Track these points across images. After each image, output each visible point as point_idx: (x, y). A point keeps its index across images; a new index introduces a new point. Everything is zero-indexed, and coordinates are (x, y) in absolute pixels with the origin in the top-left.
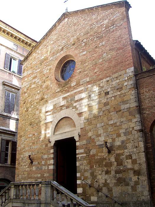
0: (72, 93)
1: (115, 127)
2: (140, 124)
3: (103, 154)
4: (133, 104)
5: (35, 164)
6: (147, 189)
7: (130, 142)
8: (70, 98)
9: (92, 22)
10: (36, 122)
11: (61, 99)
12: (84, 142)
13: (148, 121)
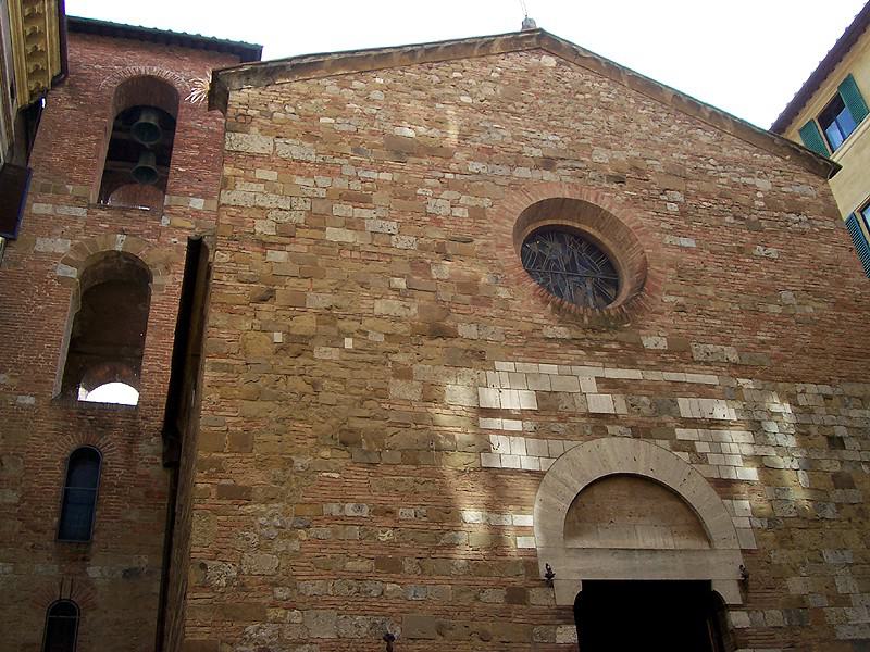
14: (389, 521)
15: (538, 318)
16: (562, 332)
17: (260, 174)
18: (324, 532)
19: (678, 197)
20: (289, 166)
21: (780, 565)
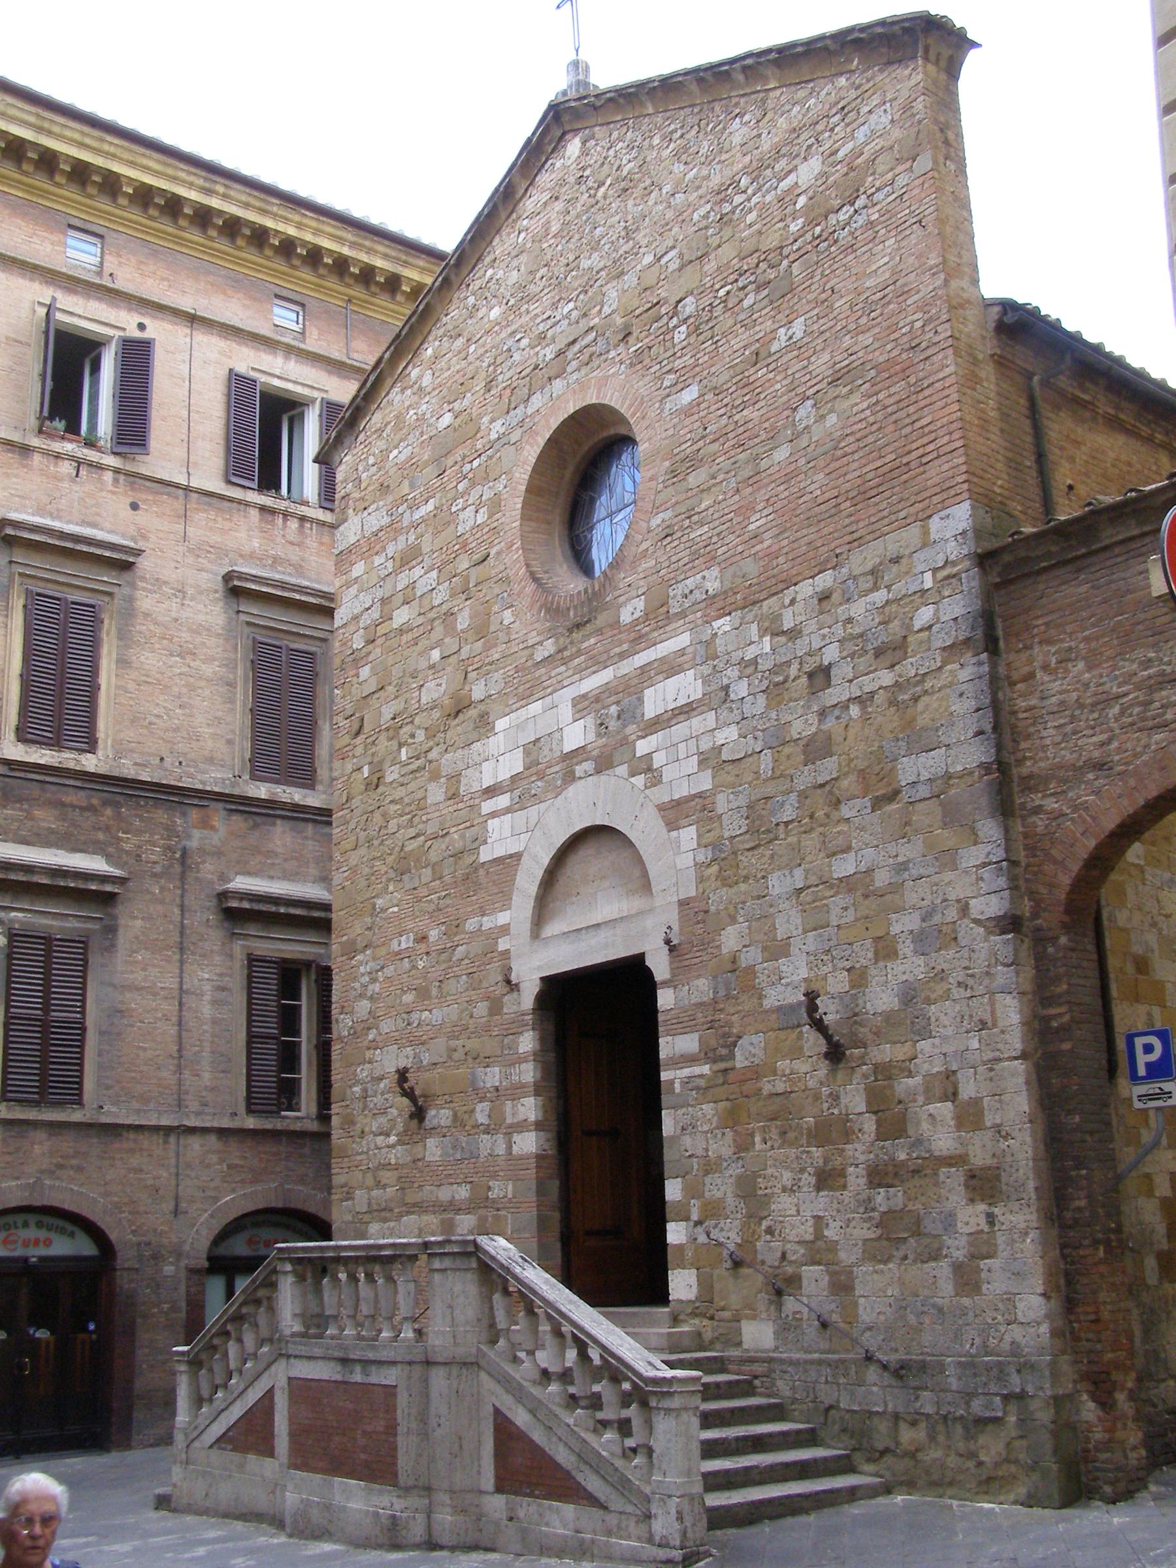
0: (629, 666)
1: (866, 896)
2: (1002, 882)
3: (802, 1066)
4: (970, 755)
6: (1038, 1283)
7: (947, 996)
8: (618, 703)
9: (728, 173)
10: (433, 856)
11: (566, 711)
12: (701, 988)
13: (1055, 862)
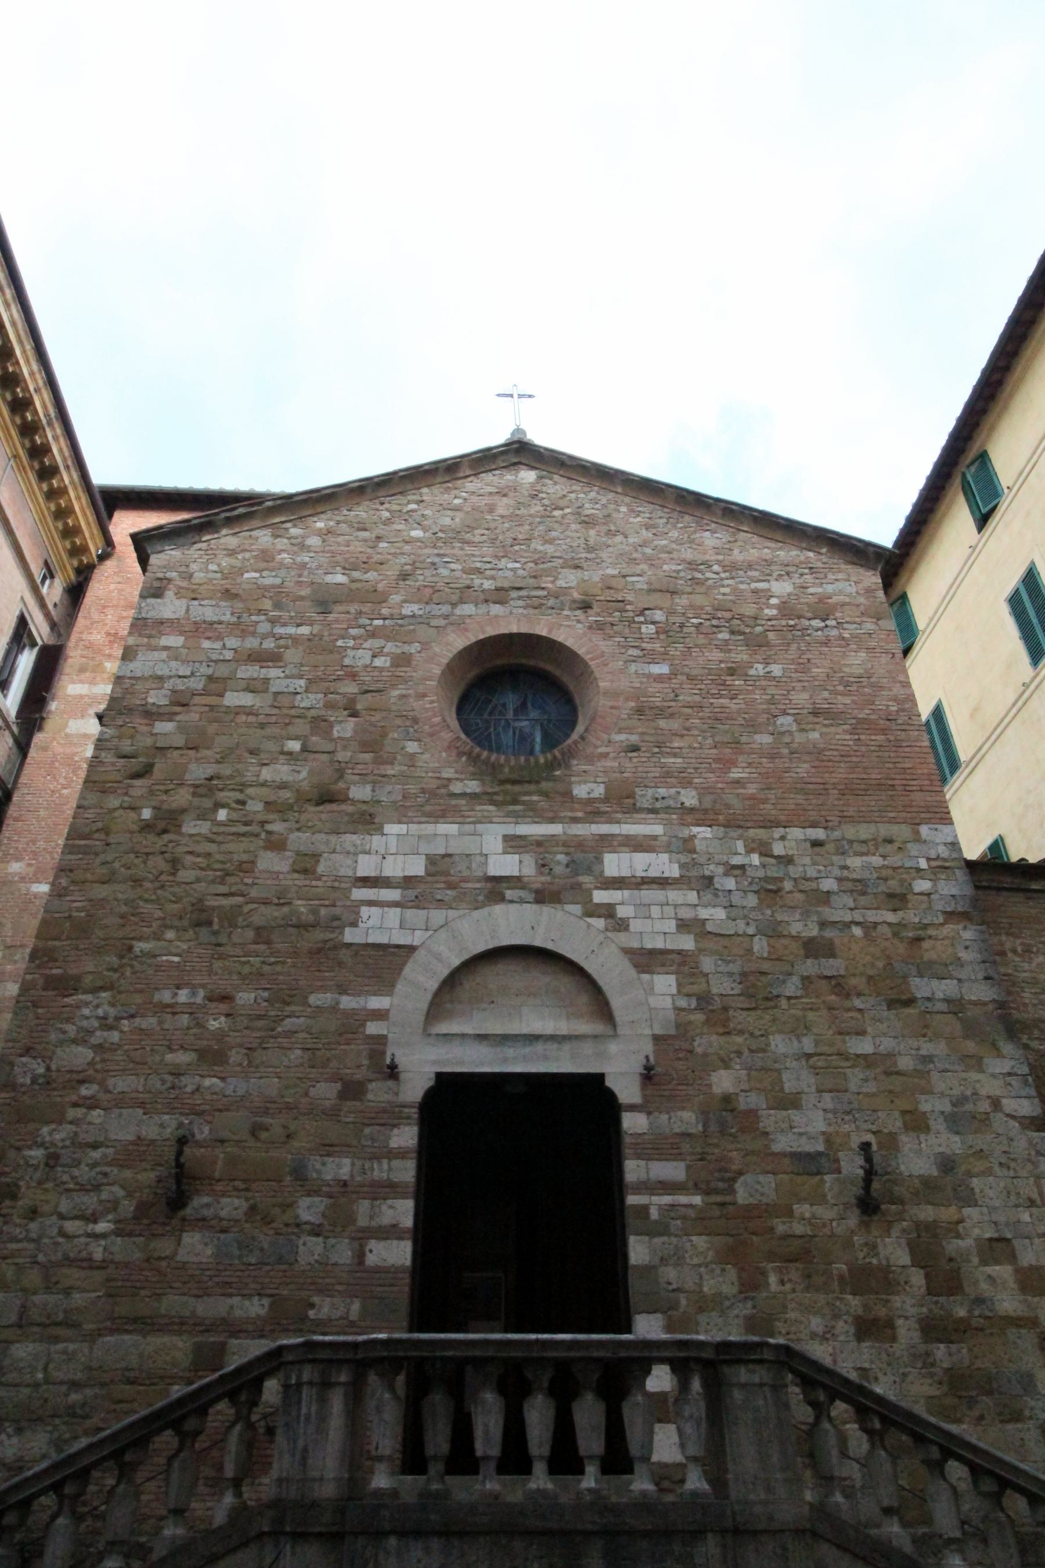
5: (206, 1212)
14: (223, 1007)
15: (448, 773)
16: (473, 786)
17: (165, 641)
18: (150, 1022)
19: (659, 616)
20: (200, 629)
21: (705, 1055)
